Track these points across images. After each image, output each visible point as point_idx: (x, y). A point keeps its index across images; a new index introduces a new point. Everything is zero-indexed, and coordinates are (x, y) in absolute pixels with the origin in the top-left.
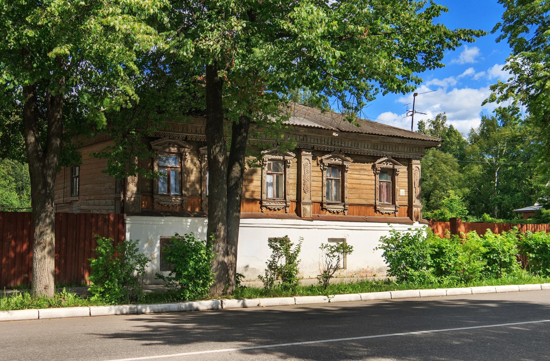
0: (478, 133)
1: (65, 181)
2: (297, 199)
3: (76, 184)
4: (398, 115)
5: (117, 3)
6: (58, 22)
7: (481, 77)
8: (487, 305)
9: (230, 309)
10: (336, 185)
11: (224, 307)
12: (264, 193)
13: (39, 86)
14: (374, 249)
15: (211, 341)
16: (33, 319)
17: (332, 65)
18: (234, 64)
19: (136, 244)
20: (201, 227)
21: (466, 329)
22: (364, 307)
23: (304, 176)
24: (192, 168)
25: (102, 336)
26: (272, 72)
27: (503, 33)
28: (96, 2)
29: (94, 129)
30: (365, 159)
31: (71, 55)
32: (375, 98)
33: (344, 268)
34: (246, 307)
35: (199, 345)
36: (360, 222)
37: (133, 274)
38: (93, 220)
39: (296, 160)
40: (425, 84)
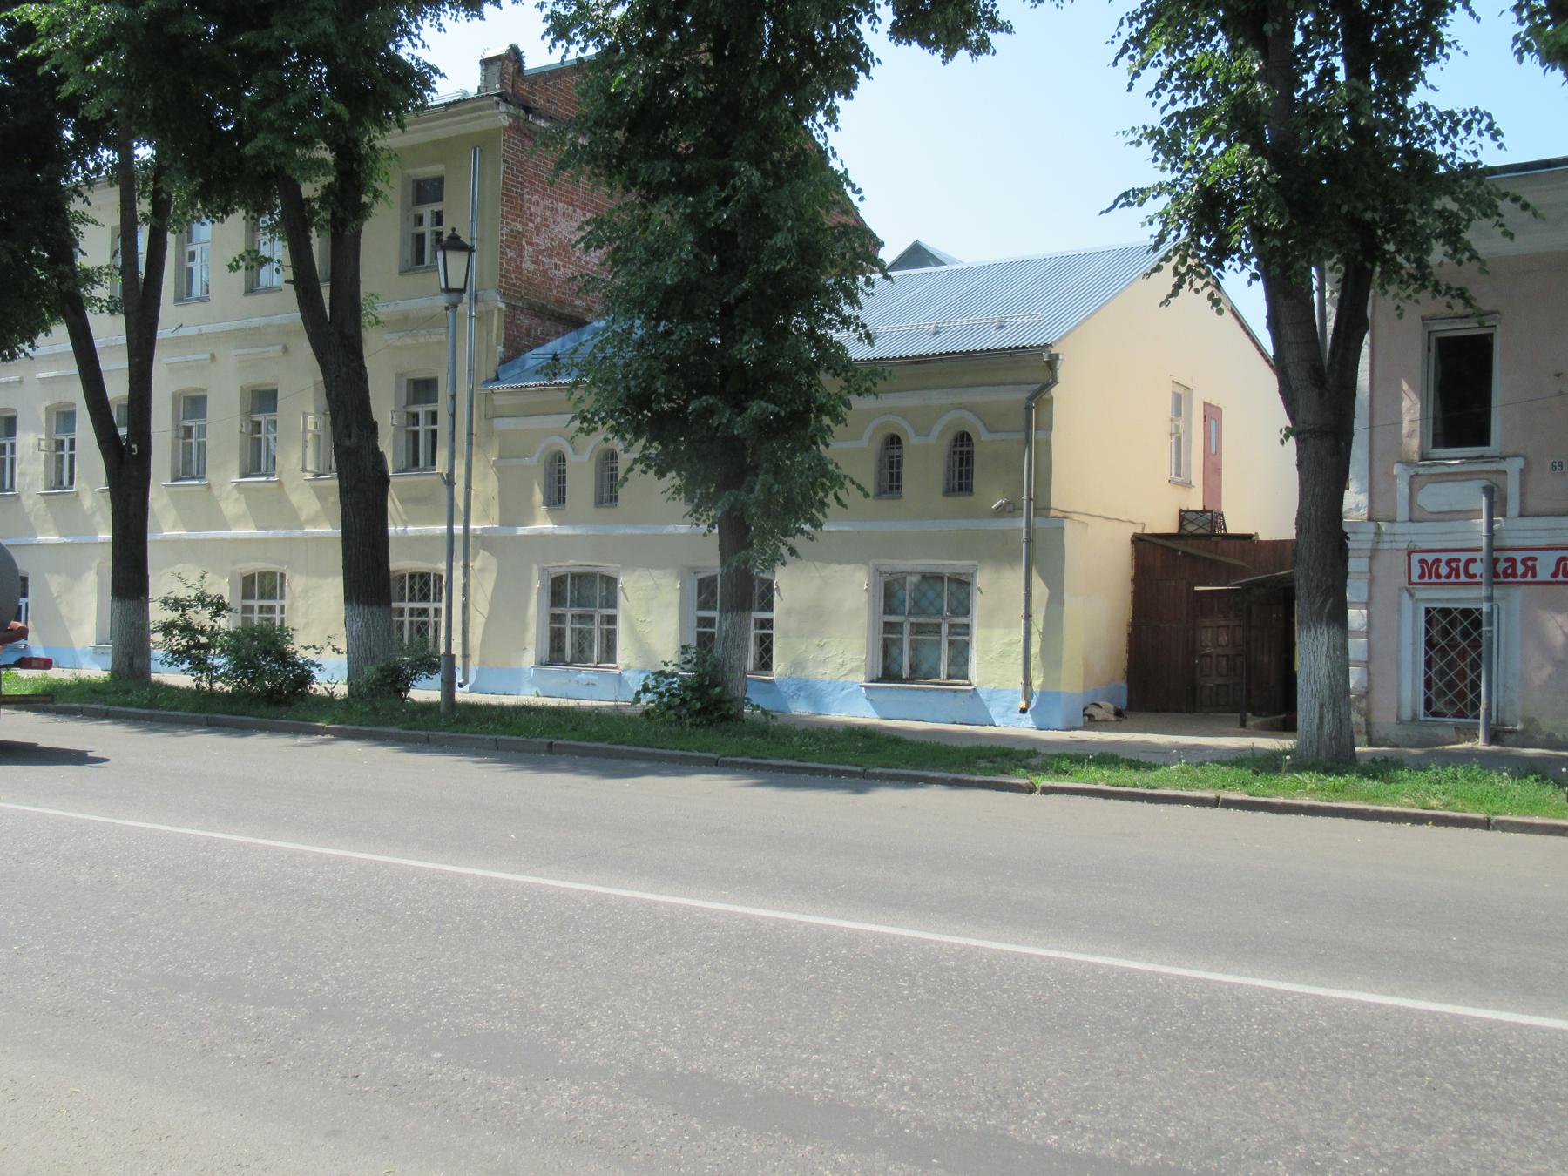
2: (31, 659)
3: (455, 123)
5: (1502, 1173)
10: (499, 314)
11: (209, 239)
15: (342, 509)
16: (1010, 384)
18: (677, 217)
19: (81, 199)
20: (710, 692)
21: (596, 748)
23: (1135, 786)
27: (844, 491)
30: (34, 698)
32: (544, 21)
35: (240, 537)
36: (1547, 164)
37: (106, 683)
38: (1480, 744)
40: (253, 228)
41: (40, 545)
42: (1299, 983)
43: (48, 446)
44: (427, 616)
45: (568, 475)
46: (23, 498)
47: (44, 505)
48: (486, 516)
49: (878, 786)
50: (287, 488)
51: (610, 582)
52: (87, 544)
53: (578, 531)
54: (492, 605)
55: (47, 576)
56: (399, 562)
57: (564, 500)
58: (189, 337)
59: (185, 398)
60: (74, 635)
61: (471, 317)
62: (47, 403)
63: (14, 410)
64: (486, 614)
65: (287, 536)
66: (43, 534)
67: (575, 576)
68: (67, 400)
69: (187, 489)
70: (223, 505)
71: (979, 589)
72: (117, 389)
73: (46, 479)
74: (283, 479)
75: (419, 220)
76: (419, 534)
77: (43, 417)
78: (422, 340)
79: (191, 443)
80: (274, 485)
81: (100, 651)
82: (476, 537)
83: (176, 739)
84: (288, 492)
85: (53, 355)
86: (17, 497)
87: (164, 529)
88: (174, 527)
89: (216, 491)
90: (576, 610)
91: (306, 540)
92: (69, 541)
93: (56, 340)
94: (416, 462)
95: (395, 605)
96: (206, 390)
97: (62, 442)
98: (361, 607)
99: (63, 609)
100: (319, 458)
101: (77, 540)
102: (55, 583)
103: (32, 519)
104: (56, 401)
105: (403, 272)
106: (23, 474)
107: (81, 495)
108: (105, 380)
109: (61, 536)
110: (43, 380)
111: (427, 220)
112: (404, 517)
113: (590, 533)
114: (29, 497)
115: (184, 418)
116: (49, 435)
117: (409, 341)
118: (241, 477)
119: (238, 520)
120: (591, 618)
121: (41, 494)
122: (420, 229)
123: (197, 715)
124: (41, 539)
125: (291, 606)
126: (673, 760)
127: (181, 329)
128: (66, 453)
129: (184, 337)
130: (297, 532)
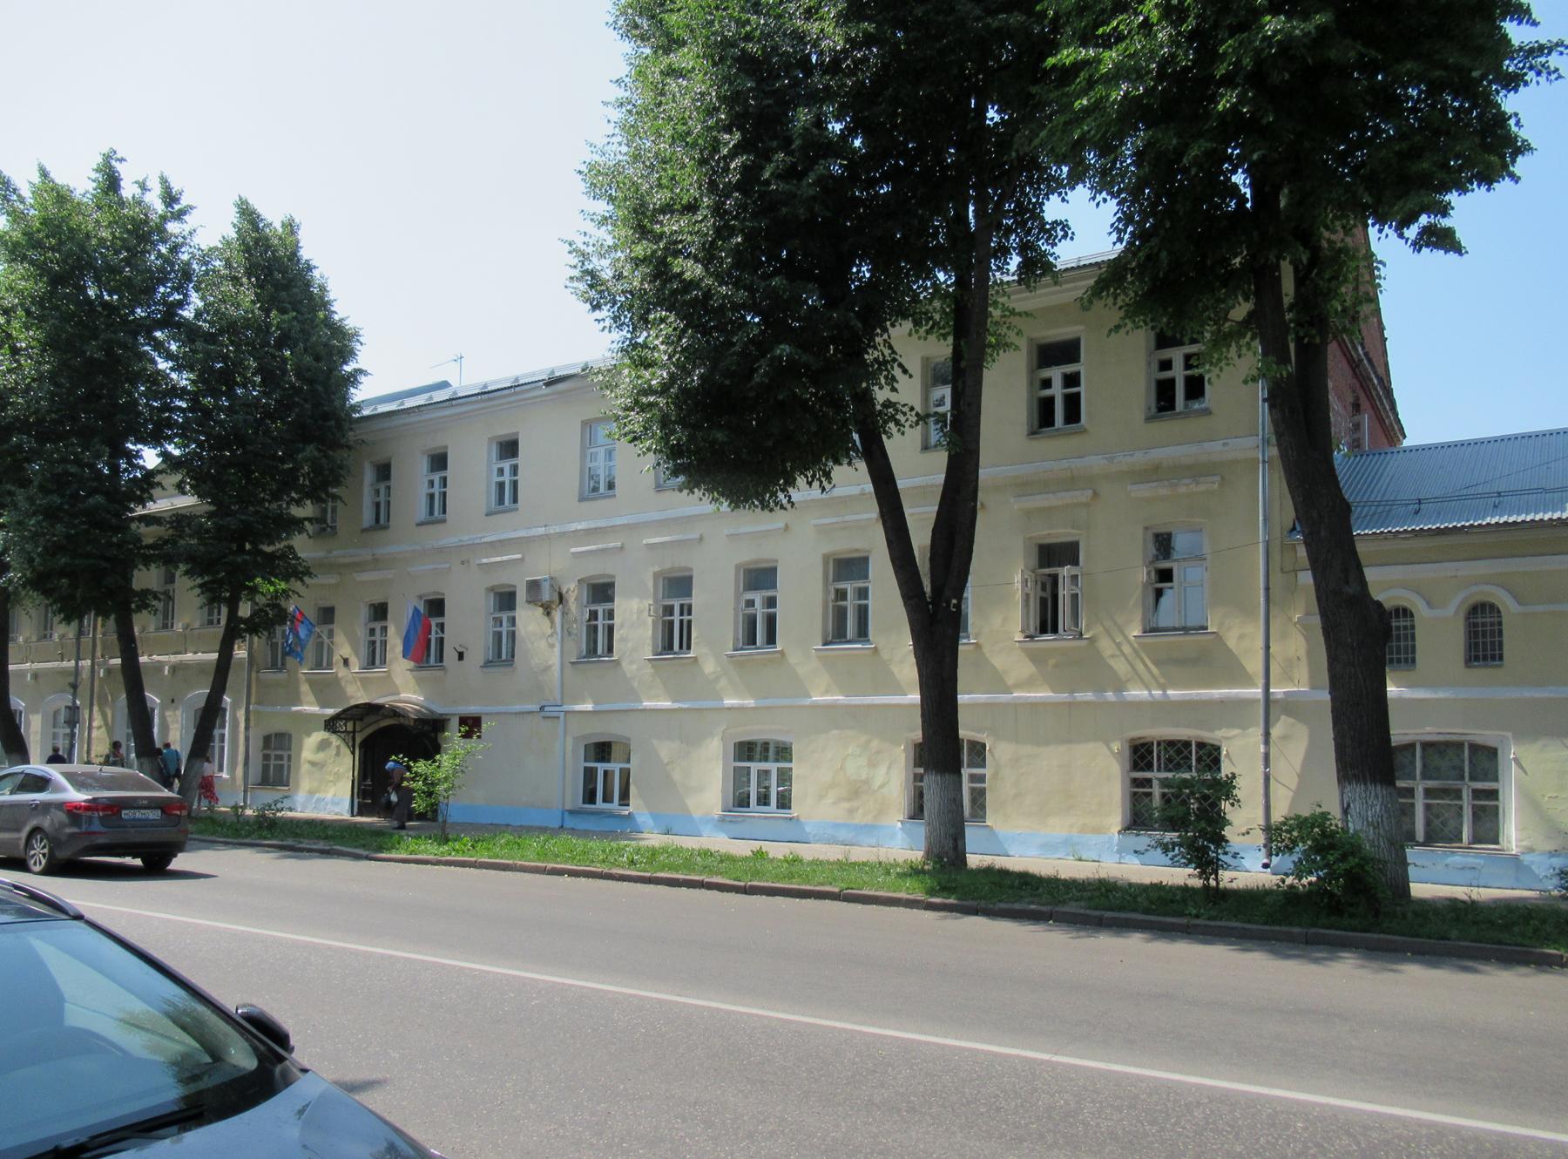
0: (1225, 806)
1: (358, 728)
4: (1521, 149)
6: (269, 325)
7: (177, 515)
8: (254, 1031)
9: (289, 853)
11: (1222, 885)
12: (431, 398)
13: (1414, 124)
14: (857, 470)
17: (292, 622)
22: (1332, 660)
24: (864, 777)
25: (1480, 490)
26: (244, 386)
28: (1509, 4)
29: (785, 501)
31: (845, 422)
33: (588, 425)
34: (116, 745)
39: (941, 349)
41: (644, 710)
42: (1159, 1070)
43: (655, 611)
44: (1151, 787)
45: (1417, 631)
46: (624, 664)
47: (652, 671)
48: (1288, 677)
49: (1182, 938)
50: (986, 650)
51: (1492, 753)
52: (707, 709)
53: (1441, 694)
54: (1301, 776)
55: (655, 742)
56: (1399, 732)
57: (1414, 661)
58: (845, 497)
59: (835, 560)
60: (691, 803)
61: (1264, 461)
62: (657, 569)
63: (515, 586)
64: (1294, 787)
65: (989, 701)
66: (650, 699)
67: (1427, 746)
68: (682, 565)
69: (848, 652)
70: (895, 669)
71: (1516, 760)
72: (921, 538)
73: (653, 646)
74: (982, 641)
75: (1166, 365)
76: (1187, 698)
77: (650, 584)
78: (1183, 490)
79: (846, 608)
80: (971, 647)
81: (728, 819)
82: (1277, 701)
83: (1313, 968)
84: (987, 655)
85: (666, 520)
86: (617, 663)
87: (812, 694)
88: (827, 692)
89: (885, 655)
90: (1431, 784)
91: (1016, 705)
92: (686, 706)
93: (853, 479)
94: (373, 663)
95: (1400, 784)
96: (777, 561)
97: (672, 607)
98: (1379, 788)
99: (677, 776)
100: (1028, 618)
101: (697, 705)
102: (665, 750)
103: (636, 685)
104: (668, 566)
105: (1032, 433)
106: (622, 639)
107: (700, 660)
108: (978, 519)
109: (673, 702)
110: (651, 546)
111: (1057, 383)
112: (1162, 680)
113: (1461, 696)
114: (632, 662)
115: (834, 581)
116: (656, 600)
117: (1163, 492)
118: (824, 645)
119: (311, 704)
120: (1457, 794)
121: (649, 660)
122: (1047, 393)
123: (1266, 927)
124: (647, 704)
125: (995, 775)
126: (226, 843)
127: (835, 489)
128: (378, 638)
129: (840, 497)
130: (1003, 698)
